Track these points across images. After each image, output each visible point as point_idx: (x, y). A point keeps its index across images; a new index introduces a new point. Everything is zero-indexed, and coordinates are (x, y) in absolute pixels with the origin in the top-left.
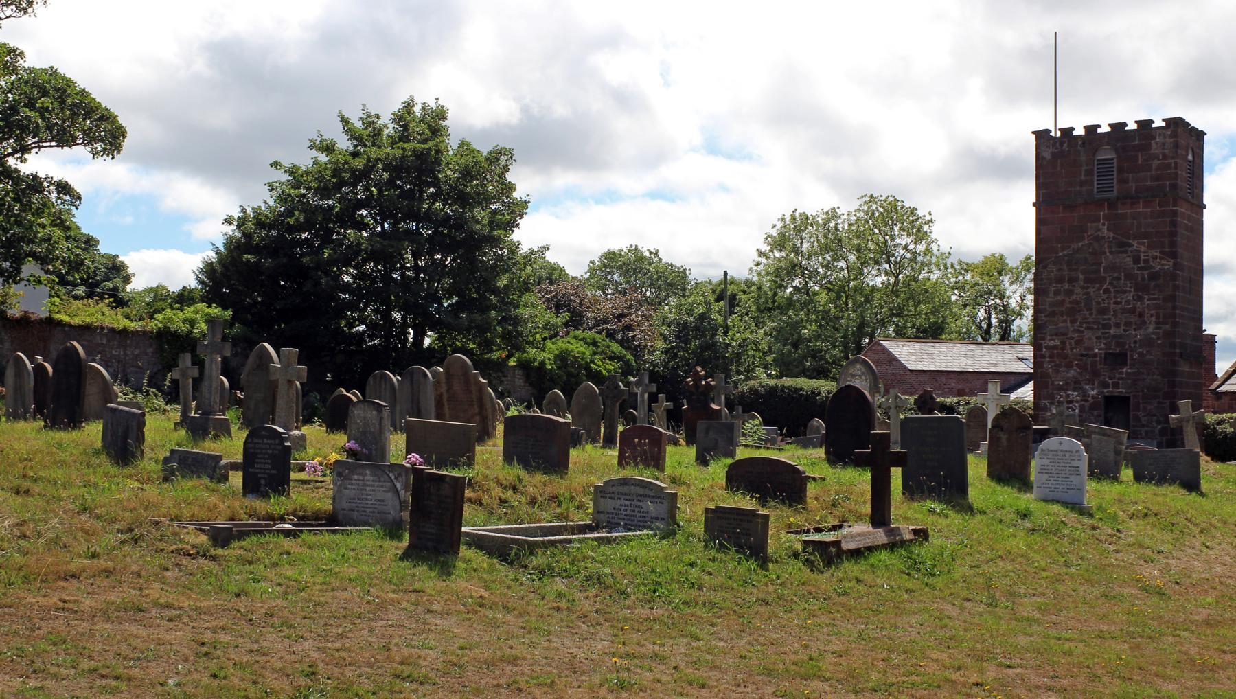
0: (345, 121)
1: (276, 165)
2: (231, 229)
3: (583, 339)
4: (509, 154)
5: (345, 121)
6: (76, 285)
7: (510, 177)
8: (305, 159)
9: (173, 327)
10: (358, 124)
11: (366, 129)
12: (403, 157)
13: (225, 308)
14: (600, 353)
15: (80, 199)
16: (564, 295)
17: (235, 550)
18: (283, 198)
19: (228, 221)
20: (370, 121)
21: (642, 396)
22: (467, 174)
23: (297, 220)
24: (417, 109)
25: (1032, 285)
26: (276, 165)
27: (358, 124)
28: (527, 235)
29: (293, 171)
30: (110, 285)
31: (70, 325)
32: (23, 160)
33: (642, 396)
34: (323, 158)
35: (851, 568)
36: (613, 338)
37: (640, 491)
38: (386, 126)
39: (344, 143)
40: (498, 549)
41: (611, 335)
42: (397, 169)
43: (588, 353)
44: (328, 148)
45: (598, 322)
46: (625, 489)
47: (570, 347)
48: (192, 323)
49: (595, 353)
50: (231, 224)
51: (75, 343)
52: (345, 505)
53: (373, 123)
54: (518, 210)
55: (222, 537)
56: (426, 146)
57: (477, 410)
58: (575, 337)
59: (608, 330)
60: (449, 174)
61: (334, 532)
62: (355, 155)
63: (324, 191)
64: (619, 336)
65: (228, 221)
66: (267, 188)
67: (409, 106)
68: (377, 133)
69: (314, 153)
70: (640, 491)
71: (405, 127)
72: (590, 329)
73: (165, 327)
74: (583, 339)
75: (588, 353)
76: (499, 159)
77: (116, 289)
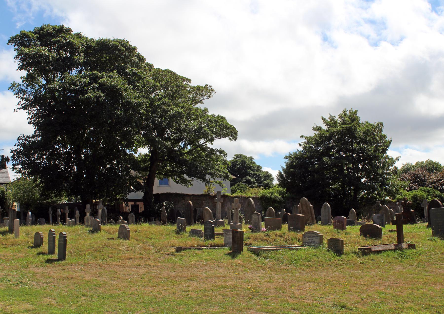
0: (324, 119)
1: (302, 137)
2: (287, 161)
3: (424, 190)
4: (382, 124)
5: (324, 119)
6: (255, 183)
7: (384, 133)
8: (312, 134)
9: (266, 195)
10: (329, 120)
11: (331, 121)
12: (342, 130)
13: (283, 188)
14: (430, 195)
15: (227, 155)
16: (417, 175)
17: (182, 253)
18: (304, 148)
19: (286, 158)
20: (332, 119)
21: (401, 209)
22: (366, 133)
23: (307, 156)
24: (348, 113)
25: (16, 179)
26: (302, 137)
27: (329, 120)
28: (391, 153)
29: (307, 138)
30: (266, 182)
31: (231, 197)
32: (212, 144)
33: (401, 209)
34: (317, 132)
35: (372, 256)
36: (437, 189)
37: (313, 235)
38: (338, 120)
39: (324, 127)
40: (256, 252)
41: (435, 188)
42: (342, 133)
43: (425, 195)
44: (319, 129)
45: (431, 183)
46: (309, 235)
47: (418, 193)
48: (272, 193)
49: (428, 195)
50: (286, 159)
51: (190, 201)
52: (226, 242)
53: (333, 119)
54: (387, 145)
55: (179, 250)
56: (351, 125)
57: (310, 215)
58: (421, 190)
59: (434, 186)
60: (360, 133)
61: (214, 249)
62: (328, 131)
63: (318, 144)
64: (439, 188)
65: (286, 158)
66: (298, 145)
67: (345, 112)
68: (335, 123)
69: (315, 132)
70: (313, 235)
71: (344, 120)
72: (428, 186)
73: (263, 195)
74: (424, 190)
75: (425, 195)
76: (378, 127)
77: (268, 183)
